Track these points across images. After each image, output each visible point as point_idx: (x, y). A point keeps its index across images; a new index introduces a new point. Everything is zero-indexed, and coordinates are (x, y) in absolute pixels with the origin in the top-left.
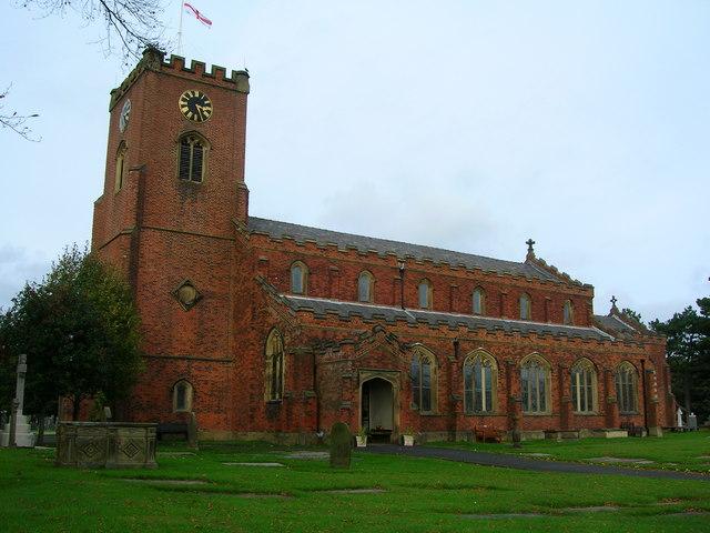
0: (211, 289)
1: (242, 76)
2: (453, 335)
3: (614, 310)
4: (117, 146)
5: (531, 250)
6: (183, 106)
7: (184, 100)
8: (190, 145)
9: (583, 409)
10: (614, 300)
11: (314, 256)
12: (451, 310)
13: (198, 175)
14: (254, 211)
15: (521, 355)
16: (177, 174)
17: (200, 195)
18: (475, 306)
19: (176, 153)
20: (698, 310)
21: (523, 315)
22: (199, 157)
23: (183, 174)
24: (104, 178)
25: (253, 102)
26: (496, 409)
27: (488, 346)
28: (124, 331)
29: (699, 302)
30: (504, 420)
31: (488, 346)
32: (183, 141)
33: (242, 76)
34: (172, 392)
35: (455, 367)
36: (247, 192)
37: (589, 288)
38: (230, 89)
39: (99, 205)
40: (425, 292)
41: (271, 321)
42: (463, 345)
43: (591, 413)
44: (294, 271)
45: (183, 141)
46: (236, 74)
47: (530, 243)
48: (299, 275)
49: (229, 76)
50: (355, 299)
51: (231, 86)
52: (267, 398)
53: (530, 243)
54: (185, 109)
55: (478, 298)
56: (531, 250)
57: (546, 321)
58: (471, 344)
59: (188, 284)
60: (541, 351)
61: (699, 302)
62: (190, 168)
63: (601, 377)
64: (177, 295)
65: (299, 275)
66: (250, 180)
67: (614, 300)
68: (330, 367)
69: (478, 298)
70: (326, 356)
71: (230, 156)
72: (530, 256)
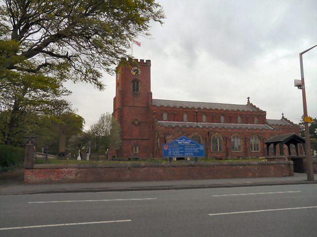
1: (149, 61)
2: (208, 130)
3: (283, 117)
4: (118, 85)
5: (248, 100)
8: (136, 82)
9: (255, 150)
10: (283, 114)
11: (169, 110)
12: (213, 122)
13: (138, 89)
14: (154, 97)
15: (231, 135)
16: (132, 90)
18: (184, 119)
21: (221, 121)
22: (138, 86)
23: (134, 90)
25: (152, 68)
26: (223, 150)
27: (219, 132)
28: (97, 45)
30: (225, 154)
31: (219, 132)
32: (133, 82)
33: (149, 61)
35: (208, 139)
36: (151, 94)
37: (265, 112)
38: (145, 66)
39: (115, 99)
40: (204, 117)
42: (210, 133)
44: (164, 115)
45: (133, 82)
46: (147, 61)
47: (248, 98)
48: (165, 116)
49: (145, 62)
50: (182, 121)
51: (146, 64)
52: (156, 149)
53: (248, 98)
55: (222, 118)
56: (248, 100)
57: (247, 124)
59: (136, 120)
60: (238, 133)
62: (135, 89)
63: (262, 140)
64: (133, 123)
65: (165, 116)
66: (152, 90)
67: (283, 114)
69: (222, 118)
72: (249, 102)
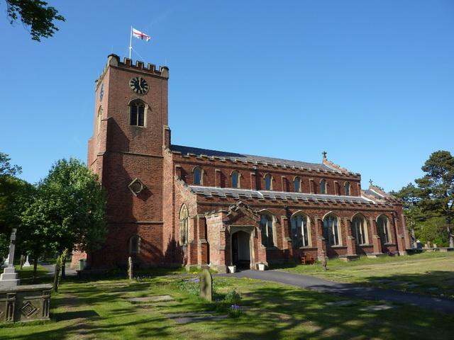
0: (152, 184)
6: (132, 86)
7: (132, 82)
13: (141, 123)
17: (143, 133)
19: (129, 111)
20: (416, 186)
24: (206, 148)
29: (416, 181)
34: (129, 241)
37: (359, 175)
41: (182, 200)
43: (337, 246)
54: (133, 87)
58: (322, 211)
61: (416, 181)
67: (371, 182)
68: (213, 225)
70: (211, 219)
71: (159, 112)
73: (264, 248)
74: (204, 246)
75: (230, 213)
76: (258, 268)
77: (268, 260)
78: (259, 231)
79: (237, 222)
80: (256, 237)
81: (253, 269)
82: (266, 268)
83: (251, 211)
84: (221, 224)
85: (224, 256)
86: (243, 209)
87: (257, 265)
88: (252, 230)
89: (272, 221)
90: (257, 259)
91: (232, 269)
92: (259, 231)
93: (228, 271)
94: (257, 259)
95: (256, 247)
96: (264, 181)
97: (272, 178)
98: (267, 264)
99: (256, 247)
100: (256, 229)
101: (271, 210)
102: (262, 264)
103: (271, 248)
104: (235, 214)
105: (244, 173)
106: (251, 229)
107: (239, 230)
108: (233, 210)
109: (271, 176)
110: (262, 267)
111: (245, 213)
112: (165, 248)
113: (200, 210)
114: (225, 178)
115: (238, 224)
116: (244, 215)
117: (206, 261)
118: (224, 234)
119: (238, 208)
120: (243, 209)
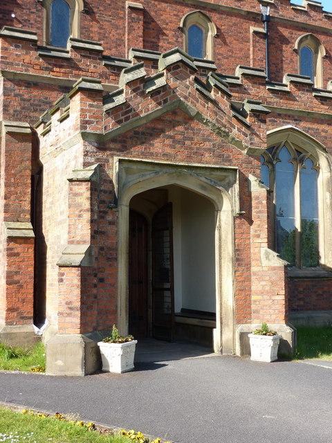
73: (280, 263)
74: (18, 248)
75: (120, 100)
76: (246, 349)
77: (293, 310)
78: (258, 190)
79: (158, 145)
80: (245, 215)
81: (229, 357)
82: (283, 353)
83: (225, 104)
84: (79, 146)
85: (77, 292)
86: (185, 88)
87: (244, 337)
88: (229, 186)
89: (317, 170)
90: (244, 311)
91: (114, 353)
92: (258, 190)
93: (96, 365)
94: (244, 311)
95: (241, 260)
96: (297, 58)
97: (322, 53)
98: (286, 333)
99: (241, 260)
100: (245, 184)
101: (317, 132)
102: (265, 332)
103: (308, 272)
104: (147, 108)
105: (227, 23)
106: (223, 176)
107: (163, 181)
108: (139, 86)
109: (318, 43)
110: (262, 349)
111: (196, 106)
112: (298, 225)
113: (15, 104)
114: (160, 32)
115: (159, 150)
116: (189, 118)
117: (29, 309)
118: (84, 190)
119: (160, 82)
120: (185, 88)
